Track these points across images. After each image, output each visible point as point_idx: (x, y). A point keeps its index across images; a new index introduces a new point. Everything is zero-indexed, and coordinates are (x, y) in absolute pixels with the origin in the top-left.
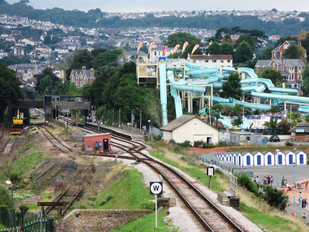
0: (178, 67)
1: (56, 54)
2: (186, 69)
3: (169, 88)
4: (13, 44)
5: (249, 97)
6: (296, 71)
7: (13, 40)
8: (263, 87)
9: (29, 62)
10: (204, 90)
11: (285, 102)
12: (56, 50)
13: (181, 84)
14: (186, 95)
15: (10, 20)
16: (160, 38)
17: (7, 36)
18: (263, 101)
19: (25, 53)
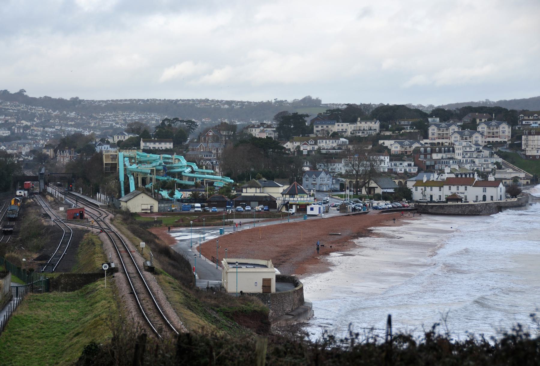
1: (46, 133)
3: (125, 170)
4: (13, 124)
5: (180, 175)
6: (217, 151)
7: (15, 121)
8: (189, 169)
9: (27, 139)
10: (150, 171)
11: (205, 180)
12: (46, 129)
14: (137, 175)
15: (12, 106)
16: (63, 291)
17: (10, 118)
19: (23, 131)
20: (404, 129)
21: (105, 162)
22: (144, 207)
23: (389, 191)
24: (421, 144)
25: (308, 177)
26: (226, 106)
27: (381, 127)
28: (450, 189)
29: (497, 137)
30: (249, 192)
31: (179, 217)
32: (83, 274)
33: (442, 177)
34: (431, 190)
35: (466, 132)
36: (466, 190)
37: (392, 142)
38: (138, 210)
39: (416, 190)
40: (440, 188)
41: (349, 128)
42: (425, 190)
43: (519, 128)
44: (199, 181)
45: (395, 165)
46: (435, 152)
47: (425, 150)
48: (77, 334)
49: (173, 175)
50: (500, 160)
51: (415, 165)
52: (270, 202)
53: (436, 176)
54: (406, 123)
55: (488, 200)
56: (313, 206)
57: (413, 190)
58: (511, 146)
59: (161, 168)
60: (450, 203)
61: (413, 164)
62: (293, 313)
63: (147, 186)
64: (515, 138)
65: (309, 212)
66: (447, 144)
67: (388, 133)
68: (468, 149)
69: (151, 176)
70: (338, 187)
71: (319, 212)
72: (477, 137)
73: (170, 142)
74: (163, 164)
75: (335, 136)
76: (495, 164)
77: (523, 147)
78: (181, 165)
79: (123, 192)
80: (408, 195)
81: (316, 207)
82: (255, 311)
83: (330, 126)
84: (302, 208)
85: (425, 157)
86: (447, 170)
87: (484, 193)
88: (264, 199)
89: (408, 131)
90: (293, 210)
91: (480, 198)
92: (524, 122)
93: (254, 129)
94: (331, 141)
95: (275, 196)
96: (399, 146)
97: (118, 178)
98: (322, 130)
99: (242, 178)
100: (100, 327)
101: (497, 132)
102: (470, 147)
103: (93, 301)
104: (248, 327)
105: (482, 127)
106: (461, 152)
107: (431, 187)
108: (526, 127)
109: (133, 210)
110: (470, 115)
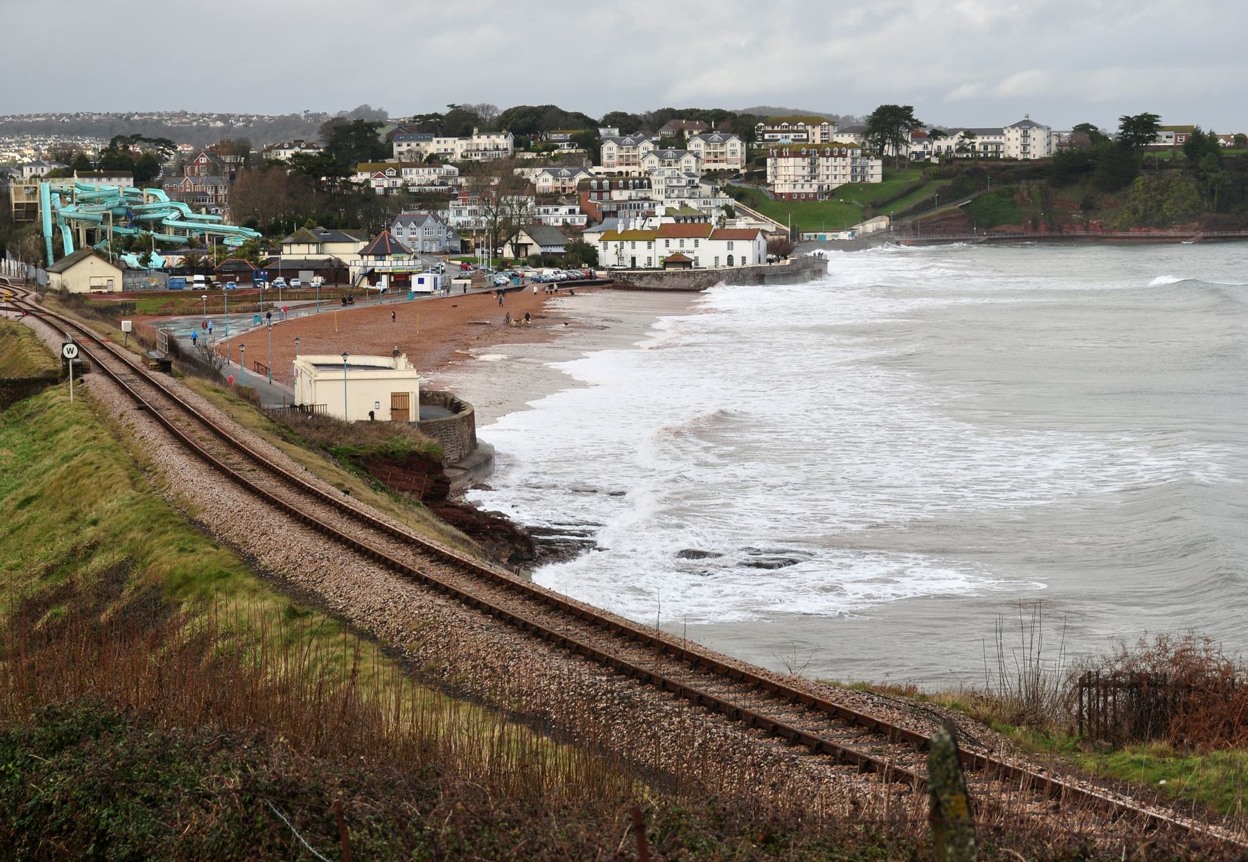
0: (65, 189)
2: (77, 191)
3: (54, 215)
5: (159, 226)
8: (176, 213)
10: (101, 218)
13: (69, 210)
18: (178, 231)
20: (557, 147)
21: (14, 202)
22: (96, 282)
23: (555, 250)
24: (590, 174)
25: (400, 226)
26: (219, 124)
27: (517, 144)
28: (667, 246)
29: (722, 161)
30: (294, 252)
31: (164, 300)
32: (9, 381)
33: (652, 224)
34: (633, 247)
35: (670, 152)
36: (696, 246)
37: (539, 171)
38: (84, 288)
39: (606, 248)
40: (649, 244)
41: (456, 147)
42: (622, 248)
43: (759, 146)
44: (195, 235)
45: (546, 212)
46: (618, 188)
47: (600, 185)
48: (27, 501)
49: (145, 225)
50: (732, 202)
51: (581, 212)
52: (335, 272)
53: (639, 221)
54: (560, 136)
55: (737, 263)
56: (421, 276)
57: (600, 248)
58: (749, 177)
59: (121, 211)
60: (668, 270)
61: (578, 209)
62: (463, 465)
63: (96, 246)
64: (753, 163)
65: (416, 287)
66: (636, 174)
67: (528, 156)
68: (675, 183)
69: (104, 227)
70: (457, 244)
71: (435, 287)
72: (688, 162)
73: (127, 176)
74: (127, 205)
75: (434, 161)
76: (723, 208)
77: (769, 180)
78: (159, 205)
79: (51, 258)
80: (590, 256)
81: (428, 278)
82: (414, 453)
83: (423, 144)
84: (401, 281)
85: (600, 198)
86: (660, 210)
87: (730, 252)
88: (326, 266)
89: (565, 151)
90: (383, 284)
91: (723, 261)
92: (767, 136)
93: (282, 152)
94: (426, 170)
95: (346, 260)
96: (550, 177)
97: (40, 232)
98: (409, 151)
99: (275, 232)
100: (86, 481)
101: (722, 153)
102: (679, 178)
103: (46, 430)
104: (403, 490)
105: (697, 144)
106: (663, 187)
107: (633, 241)
108: (771, 144)
109: (74, 289)
110: (672, 123)
